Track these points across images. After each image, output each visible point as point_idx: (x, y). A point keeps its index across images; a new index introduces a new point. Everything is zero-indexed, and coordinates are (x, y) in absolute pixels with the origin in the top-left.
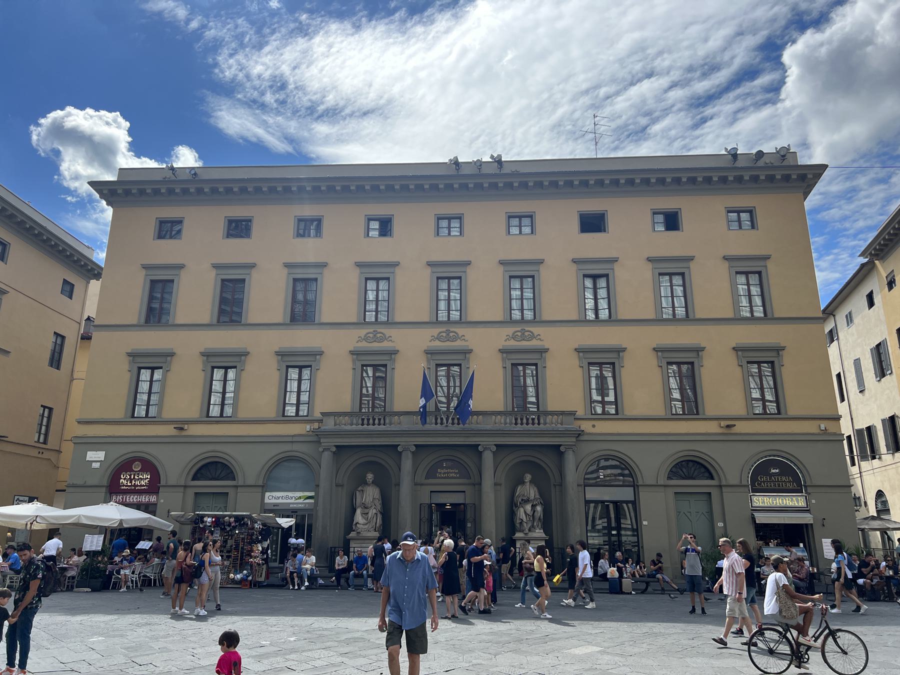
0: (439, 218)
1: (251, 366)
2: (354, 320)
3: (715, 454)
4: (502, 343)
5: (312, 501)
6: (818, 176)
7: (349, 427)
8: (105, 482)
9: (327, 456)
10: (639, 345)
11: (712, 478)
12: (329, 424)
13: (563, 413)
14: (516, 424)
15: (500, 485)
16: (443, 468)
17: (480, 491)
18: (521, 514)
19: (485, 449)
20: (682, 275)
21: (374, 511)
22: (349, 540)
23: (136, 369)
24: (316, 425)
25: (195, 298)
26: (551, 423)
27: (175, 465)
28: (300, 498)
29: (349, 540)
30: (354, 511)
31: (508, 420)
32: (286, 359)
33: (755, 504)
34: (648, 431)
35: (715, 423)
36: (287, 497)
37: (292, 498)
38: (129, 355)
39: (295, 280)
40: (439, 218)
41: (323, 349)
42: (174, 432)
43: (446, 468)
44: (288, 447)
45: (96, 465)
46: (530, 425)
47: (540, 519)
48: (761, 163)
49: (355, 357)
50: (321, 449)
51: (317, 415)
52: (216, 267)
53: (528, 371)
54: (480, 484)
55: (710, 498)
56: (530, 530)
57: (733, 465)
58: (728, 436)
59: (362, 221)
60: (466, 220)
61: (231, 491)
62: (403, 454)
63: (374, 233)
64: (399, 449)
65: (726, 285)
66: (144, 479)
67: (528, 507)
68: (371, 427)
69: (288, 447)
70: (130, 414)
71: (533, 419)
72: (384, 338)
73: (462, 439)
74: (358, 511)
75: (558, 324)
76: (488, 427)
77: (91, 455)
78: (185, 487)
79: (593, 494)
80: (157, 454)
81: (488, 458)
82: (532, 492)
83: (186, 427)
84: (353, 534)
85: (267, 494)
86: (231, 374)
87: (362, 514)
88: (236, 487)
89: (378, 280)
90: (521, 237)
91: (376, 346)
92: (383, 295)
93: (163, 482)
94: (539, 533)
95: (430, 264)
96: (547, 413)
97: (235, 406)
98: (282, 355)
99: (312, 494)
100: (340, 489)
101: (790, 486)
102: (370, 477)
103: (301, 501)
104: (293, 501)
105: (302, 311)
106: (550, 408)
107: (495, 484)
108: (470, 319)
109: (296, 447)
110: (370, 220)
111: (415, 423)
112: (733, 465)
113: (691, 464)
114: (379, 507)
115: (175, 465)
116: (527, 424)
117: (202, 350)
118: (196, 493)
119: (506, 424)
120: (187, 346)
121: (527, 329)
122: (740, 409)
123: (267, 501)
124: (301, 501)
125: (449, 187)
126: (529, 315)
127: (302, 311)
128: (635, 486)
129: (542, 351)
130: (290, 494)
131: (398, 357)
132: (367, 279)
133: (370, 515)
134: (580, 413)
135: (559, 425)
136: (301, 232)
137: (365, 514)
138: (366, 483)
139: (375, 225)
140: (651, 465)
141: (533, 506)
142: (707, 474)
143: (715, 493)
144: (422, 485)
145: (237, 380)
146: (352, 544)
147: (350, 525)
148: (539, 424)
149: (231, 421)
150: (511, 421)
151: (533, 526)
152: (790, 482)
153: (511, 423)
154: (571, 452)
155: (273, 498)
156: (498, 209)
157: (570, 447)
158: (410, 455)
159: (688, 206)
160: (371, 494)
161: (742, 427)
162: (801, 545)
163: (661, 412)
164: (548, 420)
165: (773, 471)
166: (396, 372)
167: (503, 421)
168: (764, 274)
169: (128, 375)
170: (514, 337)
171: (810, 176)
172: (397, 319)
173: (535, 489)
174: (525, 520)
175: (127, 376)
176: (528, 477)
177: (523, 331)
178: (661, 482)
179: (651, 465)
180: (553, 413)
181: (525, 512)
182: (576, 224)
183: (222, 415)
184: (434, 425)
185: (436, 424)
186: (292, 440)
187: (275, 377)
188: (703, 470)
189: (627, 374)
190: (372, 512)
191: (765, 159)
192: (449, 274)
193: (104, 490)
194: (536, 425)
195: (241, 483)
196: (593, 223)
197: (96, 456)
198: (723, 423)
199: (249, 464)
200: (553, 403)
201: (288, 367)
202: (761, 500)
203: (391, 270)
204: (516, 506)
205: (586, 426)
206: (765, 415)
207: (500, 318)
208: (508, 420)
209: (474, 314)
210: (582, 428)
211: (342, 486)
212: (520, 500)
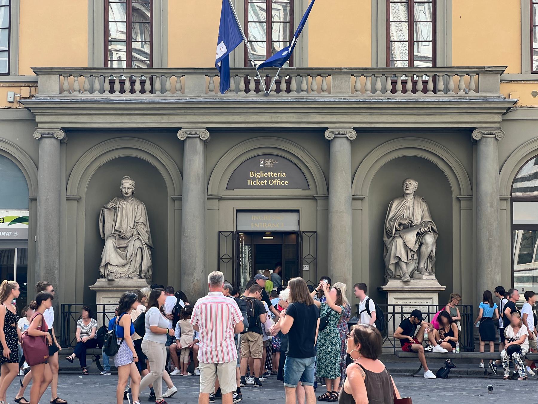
19: (337, 136)
54: (326, 198)
67: (411, 238)
73: (294, 118)
74: (110, 244)
81: (342, 151)
87: (117, 248)
144: (221, 199)
154: (491, 140)
158: (200, 147)
173: (424, 206)
174: (404, 258)
176: (412, 185)
181: (405, 246)
211: (79, 200)
212: (396, 224)
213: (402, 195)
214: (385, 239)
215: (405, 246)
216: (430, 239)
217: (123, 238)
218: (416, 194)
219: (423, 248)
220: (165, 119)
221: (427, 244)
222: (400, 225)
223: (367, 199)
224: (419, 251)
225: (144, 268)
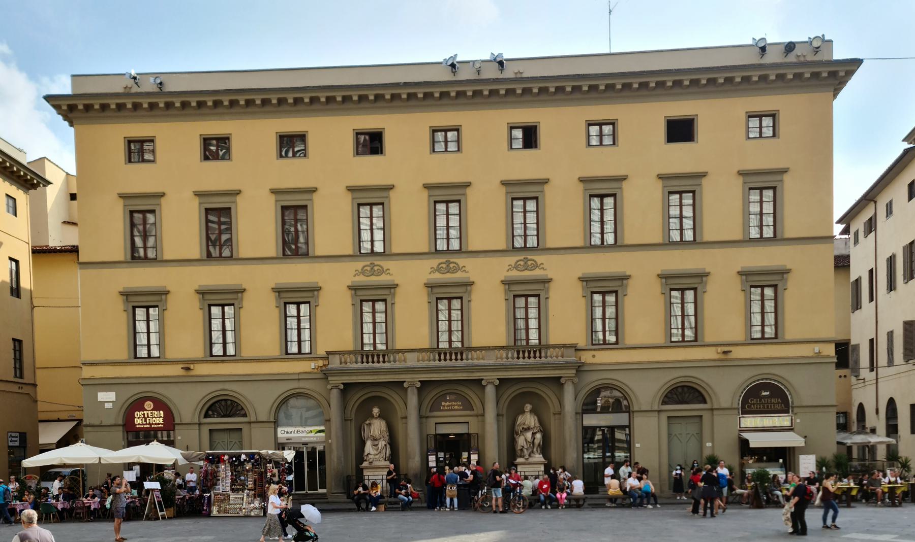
0: (434, 131)
1: (248, 301)
2: (350, 252)
3: (246, 394)
4: (504, 274)
5: (323, 434)
6: (850, 74)
7: (354, 366)
8: (120, 422)
9: (335, 394)
10: (723, 268)
11: (705, 402)
12: (335, 363)
13: (564, 346)
14: (518, 358)
15: (502, 415)
16: (446, 401)
17: (483, 421)
18: (521, 441)
20: (774, 188)
21: (384, 443)
22: (362, 469)
23: (131, 309)
24: (320, 363)
25: (181, 230)
26: (553, 356)
27: (188, 403)
28: (311, 432)
29: (362, 469)
30: (363, 443)
31: (510, 355)
32: (750, 278)
33: (742, 425)
34: (680, 358)
35: (714, 349)
36: (298, 432)
39: (132, 212)
41: (320, 285)
42: (182, 372)
43: (450, 401)
44: (295, 385)
45: (107, 406)
46: (532, 359)
47: (539, 445)
48: (792, 58)
49: (744, 277)
50: (329, 387)
51: (321, 351)
52: (198, 194)
54: (483, 415)
55: (701, 420)
56: (530, 455)
57: (726, 389)
58: (726, 362)
61: (245, 428)
62: (409, 390)
63: (518, 144)
64: (405, 385)
65: (738, 204)
66: (157, 419)
67: (529, 435)
68: (376, 365)
69: (295, 385)
70: (208, 354)
72: (382, 271)
74: (369, 444)
75: (562, 251)
76: (492, 362)
77: (102, 396)
78: (200, 424)
79: (591, 420)
80: (170, 394)
81: (490, 391)
82: (529, 419)
83: (192, 366)
84: (365, 464)
85: (279, 430)
86: (690, 295)
88: (250, 423)
89: (371, 205)
91: (527, 274)
93: (177, 421)
94: (538, 458)
95: (427, 187)
96: (548, 347)
97: (161, 345)
98: (586, 281)
99: (322, 428)
101: (778, 407)
102: (376, 411)
104: (304, 434)
105: (293, 246)
106: (474, 344)
107: (498, 415)
108: (471, 248)
109: (302, 384)
110: (512, 128)
111: (502, 358)
112: (726, 389)
113: (686, 389)
115: (188, 403)
116: (529, 358)
117: (121, 290)
118: (210, 430)
119: (507, 358)
120: (183, 284)
121: (530, 257)
122: (738, 335)
123: (279, 435)
125: (781, 77)
126: (455, 245)
127: (293, 246)
128: (628, 410)
129: (468, 285)
130: (302, 429)
131: (552, 285)
132: (359, 205)
133: (380, 446)
134: (582, 342)
135: (560, 358)
136: (283, 153)
139: (518, 134)
140: (646, 392)
142: (700, 398)
143: (706, 416)
145: (236, 318)
146: (366, 473)
147: (360, 456)
148: (540, 357)
149: (236, 359)
150: (513, 355)
151: (532, 452)
152: (778, 403)
153: (513, 358)
155: (283, 433)
156: (736, 107)
157: (569, 378)
158: (415, 391)
159: (549, 119)
160: (377, 427)
161: (739, 353)
162: (781, 461)
163: (660, 340)
164: (549, 354)
165: (764, 394)
166: (550, 301)
167: (504, 355)
168: (778, 190)
169: (277, 310)
170: (363, 272)
171: (842, 74)
172: (550, 245)
175: (350, 309)
176: (528, 407)
178: (656, 408)
179: (646, 392)
180: (554, 347)
181: (526, 440)
182: (661, 131)
183: (225, 354)
184: (437, 362)
185: (440, 360)
186: (299, 377)
187: (275, 314)
188: (697, 394)
189: (631, 304)
190: (382, 444)
191: (798, 51)
193: (121, 428)
194: (538, 359)
195: (253, 419)
196: (680, 131)
197: (107, 397)
198: (720, 349)
199: (259, 402)
200: (555, 337)
201: (362, 301)
202: (749, 421)
203: (778, 177)
204: (517, 434)
205: (587, 357)
207: (350, 252)
208: (510, 355)
209: (475, 244)
210: (583, 361)
213: (523, 412)
215: (526, 440)
216: (539, 436)
218: (531, 411)
220: (397, 376)
224: (533, 442)
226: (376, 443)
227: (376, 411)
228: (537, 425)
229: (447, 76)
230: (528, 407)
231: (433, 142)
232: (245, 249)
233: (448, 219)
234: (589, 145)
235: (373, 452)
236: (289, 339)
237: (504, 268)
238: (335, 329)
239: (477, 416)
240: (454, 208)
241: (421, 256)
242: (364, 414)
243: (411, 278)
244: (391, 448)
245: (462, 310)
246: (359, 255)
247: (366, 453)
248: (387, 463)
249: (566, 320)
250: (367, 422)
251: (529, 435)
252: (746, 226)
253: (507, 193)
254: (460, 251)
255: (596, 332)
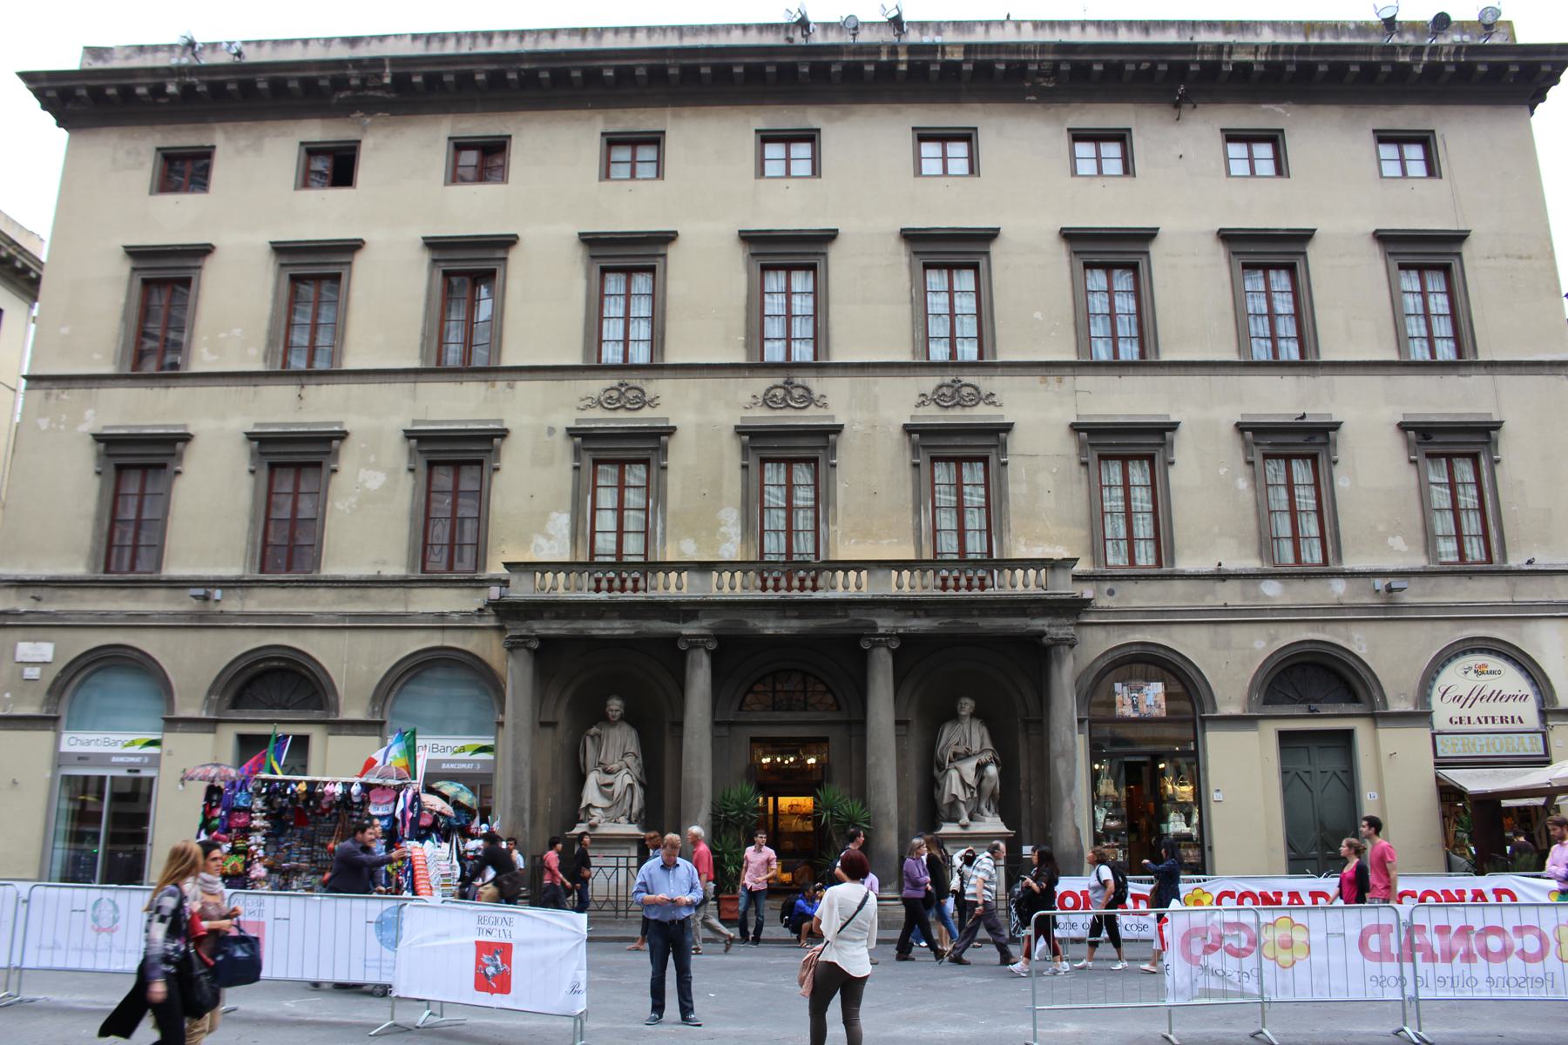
4: (567, 418)
12: (523, 589)
21: (628, 780)
25: (234, 312)
28: (463, 749)
30: (581, 780)
37: (445, 749)
38: (1404, 427)
40: (766, 137)
47: (993, 795)
53: (631, 480)
59: (751, 141)
60: (1138, 143)
67: (968, 768)
68: (617, 594)
71: (610, 581)
74: (593, 779)
80: (1190, 643)
90: (1099, 181)
92: (802, 305)
99: (490, 742)
100: (549, 731)
103: (466, 756)
104: (448, 755)
114: (636, 771)
124: (466, 756)
126: (968, 352)
137: (604, 788)
138: (603, 718)
141: (980, 768)
151: (979, 811)
161: (1413, 594)
174: (962, 797)
177: (956, 386)
190: (623, 780)
192: (314, 272)
198: (1380, 583)
203: (500, 254)
204: (941, 767)
206: (1462, 571)
211: (553, 725)
212: (949, 754)
213: (954, 717)
214: (936, 772)
216: (992, 770)
217: (607, 772)
218: (974, 715)
219: (985, 783)
221: (990, 778)
222: (955, 754)
223: (561, 728)
225: (635, 809)
226: (609, 779)
227: (615, 705)
228: (988, 745)
229: (888, 37)
230: (967, 705)
231: (761, 161)
232: (203, 359)
233: (627, 304)
234: (918, 172)
235: (600, 801)
236: (985, 535)
237: (743, 401)
238: (534, 521)
239: (848, 724)
240: (641, 283)
241: (226, 381)
242: (589, 715)
243: (704, 423)
244: (646, 797)
245: (987, 485)
246: (759, 367)
247: (583, 805)
248: (633, 829)
249: (1045, 517)
250: (594, 730)
251: (968, 768)
252: (925, 340)
253: (435, 261)
254: (979, 366)
255: (461, 545)
